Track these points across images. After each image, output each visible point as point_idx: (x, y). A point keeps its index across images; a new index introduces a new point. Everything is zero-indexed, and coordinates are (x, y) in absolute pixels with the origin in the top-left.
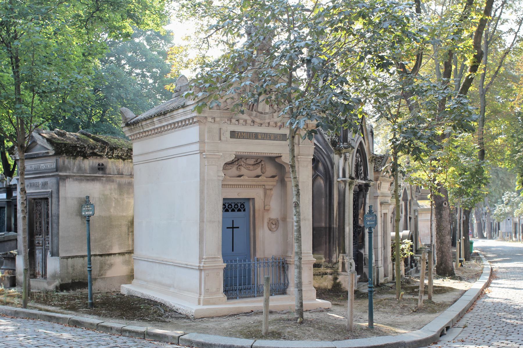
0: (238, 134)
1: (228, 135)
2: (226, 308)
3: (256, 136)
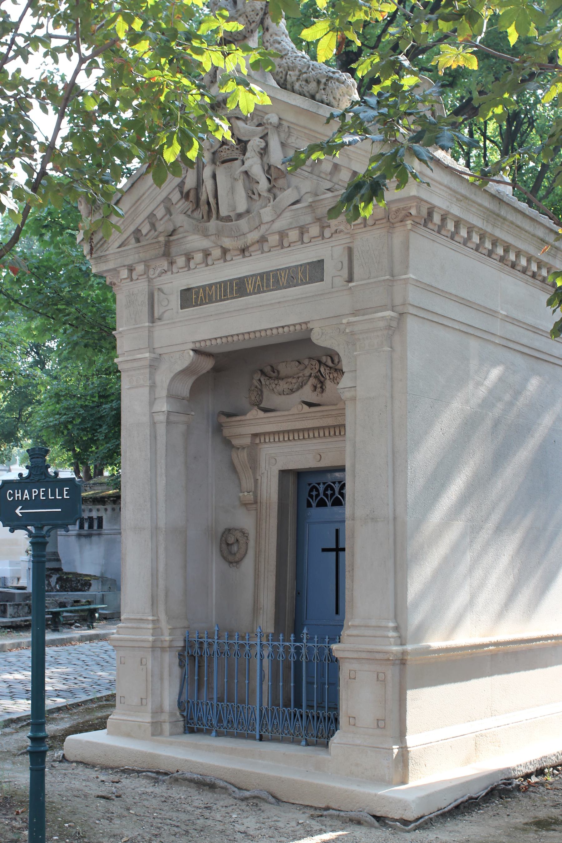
0: (197, 293)
1: (176, 300)
2: (123, 749)
3: (239, 288)
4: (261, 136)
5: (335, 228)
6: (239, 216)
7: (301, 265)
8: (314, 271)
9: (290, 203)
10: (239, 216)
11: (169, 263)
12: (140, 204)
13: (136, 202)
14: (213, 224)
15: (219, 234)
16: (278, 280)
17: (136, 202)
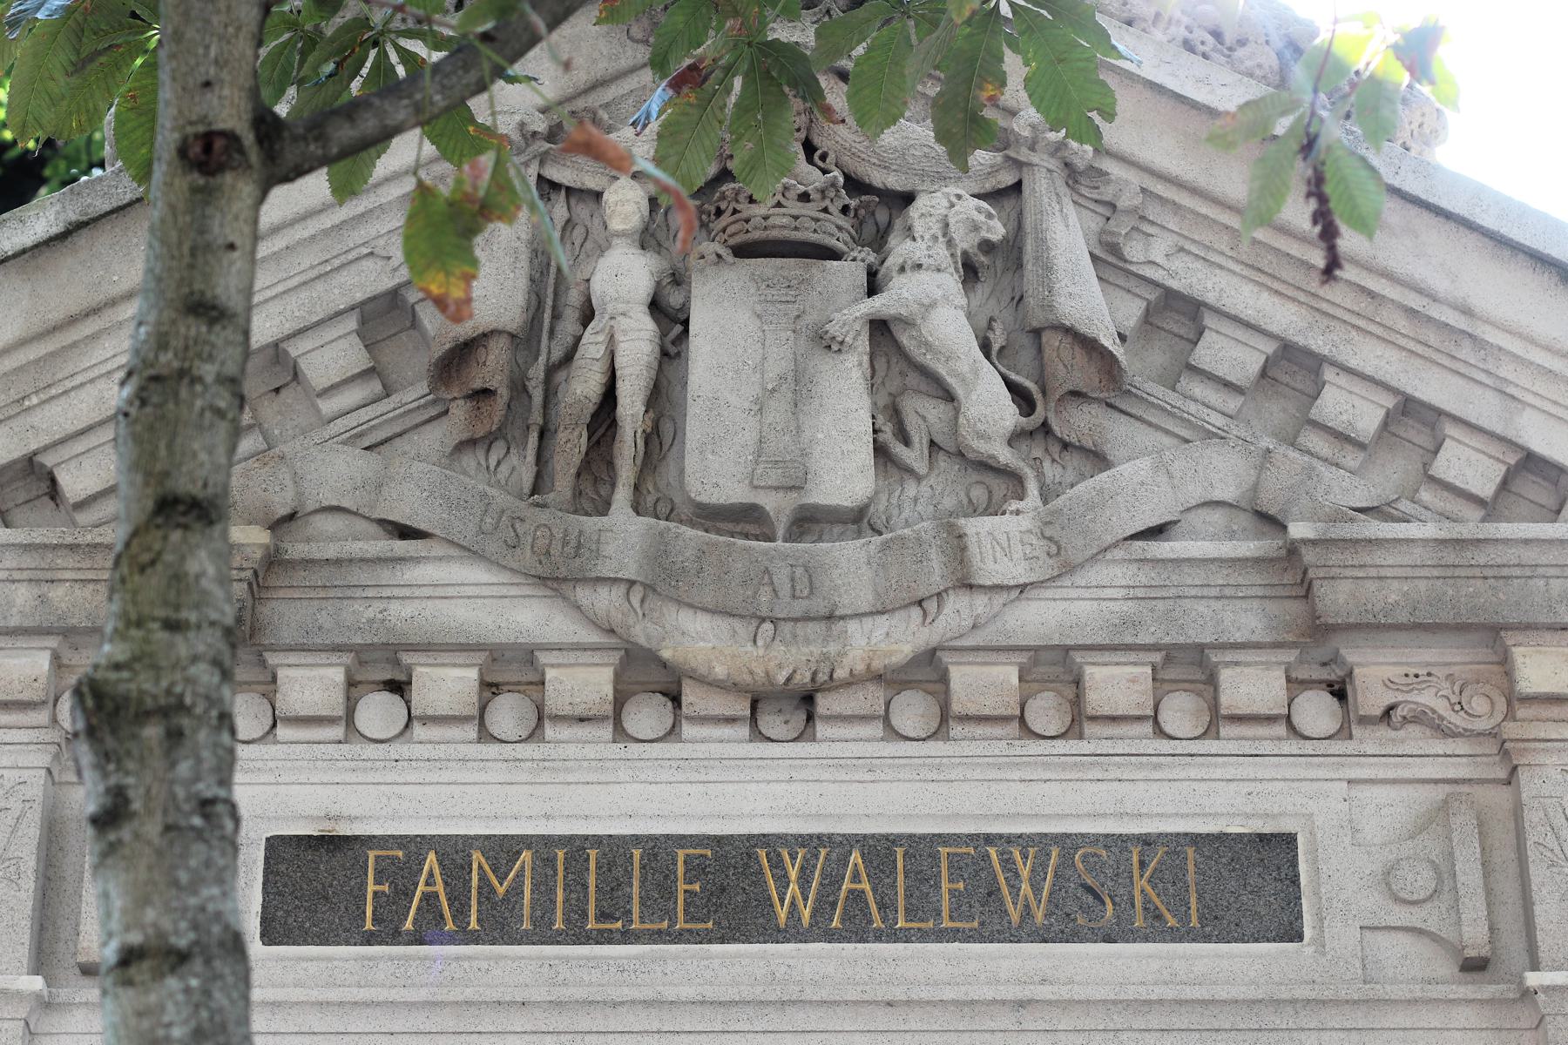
5: (1390, 698)
6: (808, 522)
7: (1146, 841)
8: (1247, 885)
9: (1140, 526)
10: (808, 522)
12: (94, 337)
13: (73, 320)
14: (623, 533)
15: (660, 582)
16: (993, 892)
17: (73, 320)
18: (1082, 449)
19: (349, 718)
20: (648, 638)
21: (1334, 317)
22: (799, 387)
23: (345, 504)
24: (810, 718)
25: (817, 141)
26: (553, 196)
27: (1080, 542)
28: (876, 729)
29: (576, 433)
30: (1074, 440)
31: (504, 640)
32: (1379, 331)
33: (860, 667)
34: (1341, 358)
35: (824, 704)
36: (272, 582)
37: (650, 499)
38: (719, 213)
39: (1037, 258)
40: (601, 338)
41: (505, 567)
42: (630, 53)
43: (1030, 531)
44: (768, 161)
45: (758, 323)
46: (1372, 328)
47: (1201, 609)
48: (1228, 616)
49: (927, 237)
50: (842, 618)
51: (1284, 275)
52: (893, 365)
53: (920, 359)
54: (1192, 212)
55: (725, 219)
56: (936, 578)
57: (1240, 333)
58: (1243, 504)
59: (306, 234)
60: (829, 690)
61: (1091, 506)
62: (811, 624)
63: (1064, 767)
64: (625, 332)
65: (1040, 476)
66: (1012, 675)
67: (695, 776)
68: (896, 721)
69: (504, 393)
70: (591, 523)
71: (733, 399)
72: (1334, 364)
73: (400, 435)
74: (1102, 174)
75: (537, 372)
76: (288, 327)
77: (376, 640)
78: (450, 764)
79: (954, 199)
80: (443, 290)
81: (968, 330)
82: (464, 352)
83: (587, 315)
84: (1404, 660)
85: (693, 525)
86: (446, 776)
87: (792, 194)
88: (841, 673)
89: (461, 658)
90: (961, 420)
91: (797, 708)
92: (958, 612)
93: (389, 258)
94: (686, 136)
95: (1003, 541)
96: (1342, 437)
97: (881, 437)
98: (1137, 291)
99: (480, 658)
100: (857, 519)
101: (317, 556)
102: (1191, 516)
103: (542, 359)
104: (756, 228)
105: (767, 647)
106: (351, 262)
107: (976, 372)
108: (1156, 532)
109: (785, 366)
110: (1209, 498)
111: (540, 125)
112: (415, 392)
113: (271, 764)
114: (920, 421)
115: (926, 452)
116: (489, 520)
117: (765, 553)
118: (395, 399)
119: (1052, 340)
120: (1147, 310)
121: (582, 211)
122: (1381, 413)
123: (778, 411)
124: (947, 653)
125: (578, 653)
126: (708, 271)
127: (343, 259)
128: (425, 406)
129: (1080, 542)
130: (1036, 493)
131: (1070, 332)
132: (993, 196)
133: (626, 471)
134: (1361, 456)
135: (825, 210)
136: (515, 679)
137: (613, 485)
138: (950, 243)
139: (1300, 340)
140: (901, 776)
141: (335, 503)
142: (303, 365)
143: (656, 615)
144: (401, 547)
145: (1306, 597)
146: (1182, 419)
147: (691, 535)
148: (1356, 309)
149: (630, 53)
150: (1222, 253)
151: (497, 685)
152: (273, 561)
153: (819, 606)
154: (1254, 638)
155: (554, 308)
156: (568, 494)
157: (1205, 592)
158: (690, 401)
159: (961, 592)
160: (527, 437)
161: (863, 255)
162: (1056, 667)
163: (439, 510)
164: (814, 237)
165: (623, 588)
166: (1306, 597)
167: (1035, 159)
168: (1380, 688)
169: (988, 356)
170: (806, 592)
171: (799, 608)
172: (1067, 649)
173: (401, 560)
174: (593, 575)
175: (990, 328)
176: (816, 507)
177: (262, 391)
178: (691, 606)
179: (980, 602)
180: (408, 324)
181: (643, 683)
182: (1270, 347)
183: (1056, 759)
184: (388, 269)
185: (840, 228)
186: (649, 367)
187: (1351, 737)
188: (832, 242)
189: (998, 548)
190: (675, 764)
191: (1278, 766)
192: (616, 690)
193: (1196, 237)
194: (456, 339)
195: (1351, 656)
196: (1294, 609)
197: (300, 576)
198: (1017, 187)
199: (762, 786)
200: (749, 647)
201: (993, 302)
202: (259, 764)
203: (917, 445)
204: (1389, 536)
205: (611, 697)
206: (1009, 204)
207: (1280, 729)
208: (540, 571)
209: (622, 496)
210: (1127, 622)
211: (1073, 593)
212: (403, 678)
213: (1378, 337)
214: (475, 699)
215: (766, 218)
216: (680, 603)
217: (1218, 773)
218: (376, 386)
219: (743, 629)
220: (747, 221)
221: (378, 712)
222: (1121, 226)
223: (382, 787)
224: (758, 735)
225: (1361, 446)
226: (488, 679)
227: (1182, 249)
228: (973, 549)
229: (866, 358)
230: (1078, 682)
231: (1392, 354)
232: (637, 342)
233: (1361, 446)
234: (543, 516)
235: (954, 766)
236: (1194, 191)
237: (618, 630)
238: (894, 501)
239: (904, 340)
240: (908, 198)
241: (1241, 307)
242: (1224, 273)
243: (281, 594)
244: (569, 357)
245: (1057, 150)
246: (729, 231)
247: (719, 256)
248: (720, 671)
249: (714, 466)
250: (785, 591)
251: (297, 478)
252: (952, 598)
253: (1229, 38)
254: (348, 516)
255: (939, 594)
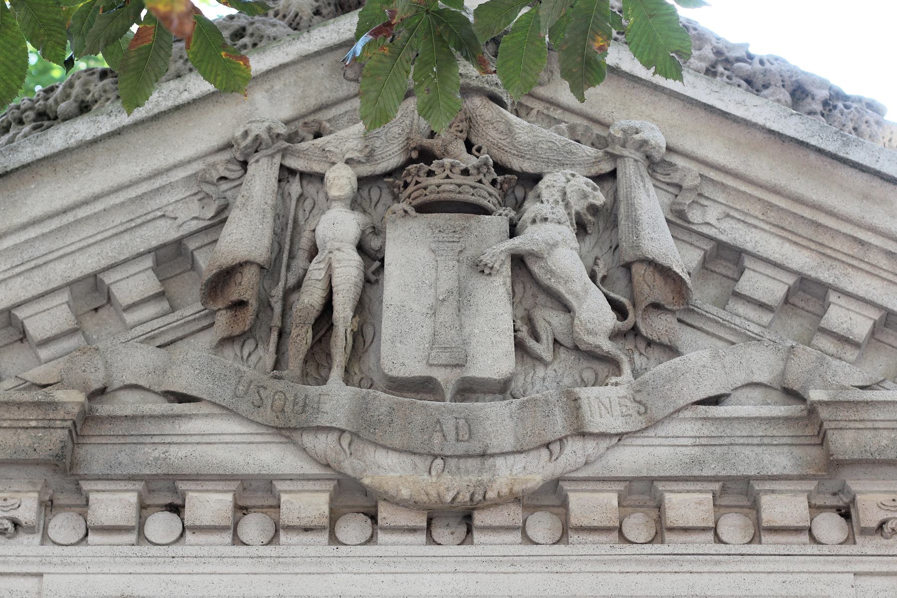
4: (594, 171)
5: (882, 515)
6: (469, 389)
10: (469, 389)
11: (41, 503)
14: (336, 397)
15: (362, 431)
18: (661, 345)
19: (140, 529)
20: (354, 469)
21: (835, 259)
22: (461, 298)
23: (141, 383)
24: (469, 531)
25: (474, 140)
26: (291, 180)
27: (661, 404)
28: (517, 537)
29: (304, 330)
30: (655, 338)
31: (251, 472)
32: (868, 268)
33: (505, 491)
34: (841, 285)
35: (479, 518)
36: (86, 432)
37: (356, 379)
38: (406, 185)
39: (628, 217)
40: (322, 266)
41: (252, 421)
42: (345, 87)
43: (625, 397)
44: (441, 103)
45: (433, 256)
46: (862, 266)
47: (747, 452)
48: (767, 458)
49: (551, 200)
50: (492, 455)
51: (800, 231)
52: (528, 290)
53: (547, 282)
54: (735, 190)
55: (411, 188)
56: (559, 428)
57: (770, 271)
58: (775, 385)
59: (118, 201)
60: (483, 509)
61: (669, 380)
62: (470, 460)
63: (651, 563)
64: (339, 261)
65: (632, 361)
66: (614, 499)
67: (386, 569)
68: (530, 533)
69: (253, 304)
70: (313, 390)
71: (415, 307)
72: (837, 290)
73: (181, 339)
74: (671, 165)
75: (278, 292)
76: (104, 263)
77: (159, 471)
78: (212, 560)
79: (569, 177)
80: (168, 8)
81: (580, 263)
82: (226, 276)
83: (314, 252)
84: (892, 489)
85: (385, 392)
86: (208, 569)
87: (457, 170)
88: (491, 495)
89: (221, 486)
90: (576, 322)
91: (460, 523)
92: (575, 452)
93: (176, 218)
94: (382, 78)
95: (607, 403)
96: (844, 340)
97: (519, 334)
98: (698, 244)
99: (234, 485)
100: (502, 389)
101: (119, 413)
102: (738, 393)
103: (281, 284)
104: (431, 193)
105: (438, 476)
106: (149, 221)
107: (586, 291)
108: (715, 401)
109: (452, 284)
110: (750, 380)
111: (282, 130)
112: (192, 307)
113: (83, 560)
114: (547, 325)
115: (551, 346)
116: (241, 388)
117: (438, 409)
118: (178, 314)
119: (639, 270)
120: (704, 258)
121: (311, 189)
122: (870, 323)
123: (446, 314)
124: (567, 483)
125: (304, 483)
126: (398, 222)
127: (143, 219)
128: (199, 319)
129: (661, 404)
130: (629, 371)
131: (652, 263)
132: (598, 178)
133: (339, 357)
134: (857, 353)
135: (480, 181)
136: (259, 503)
137: (330, 369)
138: (567, 206)
139: (813, 274)
140: (534, 569)
141: (134, 382)
142: (114, 289)
143: (359, 454)
144: (178, 408)
145: (821, 444)
146: (730, 328)
147: (384, 399)
148: (851, 253)
149: (345, 87)
150: (756, 218)
151: (246, 508)
152: (87, 417)
153: (476, 446)
154: (786, 472)
155: (290, 252)
156: (298, 372)
157: (750, 441)
158: (384, 308)
159: (577, 439)
160: (269, 337)
161: (506, 212)
162: (643, 494)
163: (206, 382)
164: (472, 199)
165: (336, 435)
166: (821, 444)
167: (625, 152)
168: (876, 509)
169: (594, 281)
170: (466, 437)
171: (461, 448)
172: (652, 480)
173: (179, 416)
174: (315, 424)
175: (596, 264)
176: (473, 380)
177: (86, 309)
178: (385, 447)
179: (591, 447)
180: (189, 267)
181: (353, 507)
182: (791, 280)
183: (645, 557)
184: (175, 225)
185: (490, 195)
186: (356, 285)
187: (855, 543)
188: (484, 202)
189: (602, 408)
190: (373, 560)
191: (805, 562)
192: (331, 510)
193: (738, 207)
194: (220, 266)
195: (854, 486)
196: (816, 452)
197: (106, 428)
198: (613, 174)
199: (435, 576)
200: (426, 476)
201: (597, 250)
202: (74, 560)
203: (545, 341)
204: (881, 399)
205: (327, 513)
206: (608, 185)
207: (805, 538)
208: (277, 423)
209: (336, 373)
210: (694, 461)
211: (656, 441)
212: (178, 502)
213: (867, 272)
214: (230, 514)
215: (438, 186)
216: (377, 445)
217: (761, 568)
218: (165, 305)
219: (422, 463)
220: (425, 188)
221: (161, 525)
222: (686, 199)
223: (163, 577)
224: (431, 541)
225: (856, 345)
226: (241, 503)
227: (728, 216)
228: (585, 408)
229: (509, 280)
230: (660, 507)
231: (876, 283)
232: (348, 270)
233: (856, 345)
234: (280, 385)
235: (572, 561)
236: (736, 176)
237: (332, 464)
238: (529, 380)
239: (535, 268)
240: (536, 178)
241: (770, 252)
242: (758, 231)
243: (93, 440)
244: (298, 285)
245: (641, 146)
246: (413, 196)
247: (406, 212)
248: (405, 493)
249: (402, 349)
250: (451, 436)
251: (107, 365)
252: (570, 443)
253: (759, 83)
254: (142, 392)
255: (561, 440)
